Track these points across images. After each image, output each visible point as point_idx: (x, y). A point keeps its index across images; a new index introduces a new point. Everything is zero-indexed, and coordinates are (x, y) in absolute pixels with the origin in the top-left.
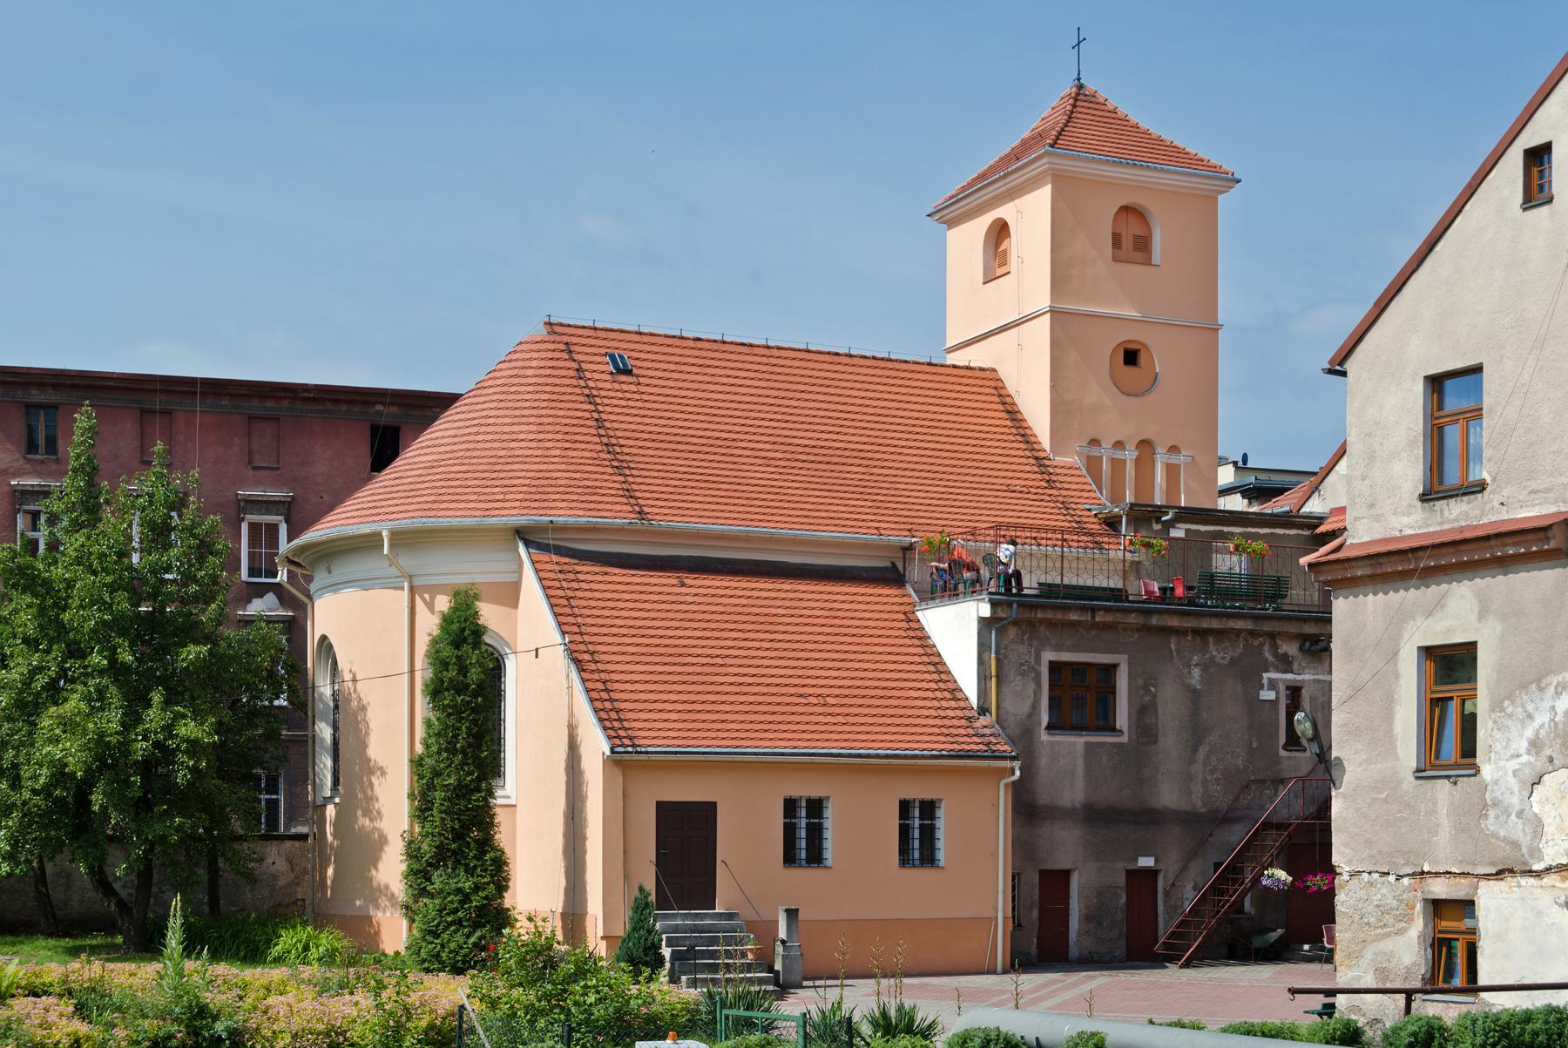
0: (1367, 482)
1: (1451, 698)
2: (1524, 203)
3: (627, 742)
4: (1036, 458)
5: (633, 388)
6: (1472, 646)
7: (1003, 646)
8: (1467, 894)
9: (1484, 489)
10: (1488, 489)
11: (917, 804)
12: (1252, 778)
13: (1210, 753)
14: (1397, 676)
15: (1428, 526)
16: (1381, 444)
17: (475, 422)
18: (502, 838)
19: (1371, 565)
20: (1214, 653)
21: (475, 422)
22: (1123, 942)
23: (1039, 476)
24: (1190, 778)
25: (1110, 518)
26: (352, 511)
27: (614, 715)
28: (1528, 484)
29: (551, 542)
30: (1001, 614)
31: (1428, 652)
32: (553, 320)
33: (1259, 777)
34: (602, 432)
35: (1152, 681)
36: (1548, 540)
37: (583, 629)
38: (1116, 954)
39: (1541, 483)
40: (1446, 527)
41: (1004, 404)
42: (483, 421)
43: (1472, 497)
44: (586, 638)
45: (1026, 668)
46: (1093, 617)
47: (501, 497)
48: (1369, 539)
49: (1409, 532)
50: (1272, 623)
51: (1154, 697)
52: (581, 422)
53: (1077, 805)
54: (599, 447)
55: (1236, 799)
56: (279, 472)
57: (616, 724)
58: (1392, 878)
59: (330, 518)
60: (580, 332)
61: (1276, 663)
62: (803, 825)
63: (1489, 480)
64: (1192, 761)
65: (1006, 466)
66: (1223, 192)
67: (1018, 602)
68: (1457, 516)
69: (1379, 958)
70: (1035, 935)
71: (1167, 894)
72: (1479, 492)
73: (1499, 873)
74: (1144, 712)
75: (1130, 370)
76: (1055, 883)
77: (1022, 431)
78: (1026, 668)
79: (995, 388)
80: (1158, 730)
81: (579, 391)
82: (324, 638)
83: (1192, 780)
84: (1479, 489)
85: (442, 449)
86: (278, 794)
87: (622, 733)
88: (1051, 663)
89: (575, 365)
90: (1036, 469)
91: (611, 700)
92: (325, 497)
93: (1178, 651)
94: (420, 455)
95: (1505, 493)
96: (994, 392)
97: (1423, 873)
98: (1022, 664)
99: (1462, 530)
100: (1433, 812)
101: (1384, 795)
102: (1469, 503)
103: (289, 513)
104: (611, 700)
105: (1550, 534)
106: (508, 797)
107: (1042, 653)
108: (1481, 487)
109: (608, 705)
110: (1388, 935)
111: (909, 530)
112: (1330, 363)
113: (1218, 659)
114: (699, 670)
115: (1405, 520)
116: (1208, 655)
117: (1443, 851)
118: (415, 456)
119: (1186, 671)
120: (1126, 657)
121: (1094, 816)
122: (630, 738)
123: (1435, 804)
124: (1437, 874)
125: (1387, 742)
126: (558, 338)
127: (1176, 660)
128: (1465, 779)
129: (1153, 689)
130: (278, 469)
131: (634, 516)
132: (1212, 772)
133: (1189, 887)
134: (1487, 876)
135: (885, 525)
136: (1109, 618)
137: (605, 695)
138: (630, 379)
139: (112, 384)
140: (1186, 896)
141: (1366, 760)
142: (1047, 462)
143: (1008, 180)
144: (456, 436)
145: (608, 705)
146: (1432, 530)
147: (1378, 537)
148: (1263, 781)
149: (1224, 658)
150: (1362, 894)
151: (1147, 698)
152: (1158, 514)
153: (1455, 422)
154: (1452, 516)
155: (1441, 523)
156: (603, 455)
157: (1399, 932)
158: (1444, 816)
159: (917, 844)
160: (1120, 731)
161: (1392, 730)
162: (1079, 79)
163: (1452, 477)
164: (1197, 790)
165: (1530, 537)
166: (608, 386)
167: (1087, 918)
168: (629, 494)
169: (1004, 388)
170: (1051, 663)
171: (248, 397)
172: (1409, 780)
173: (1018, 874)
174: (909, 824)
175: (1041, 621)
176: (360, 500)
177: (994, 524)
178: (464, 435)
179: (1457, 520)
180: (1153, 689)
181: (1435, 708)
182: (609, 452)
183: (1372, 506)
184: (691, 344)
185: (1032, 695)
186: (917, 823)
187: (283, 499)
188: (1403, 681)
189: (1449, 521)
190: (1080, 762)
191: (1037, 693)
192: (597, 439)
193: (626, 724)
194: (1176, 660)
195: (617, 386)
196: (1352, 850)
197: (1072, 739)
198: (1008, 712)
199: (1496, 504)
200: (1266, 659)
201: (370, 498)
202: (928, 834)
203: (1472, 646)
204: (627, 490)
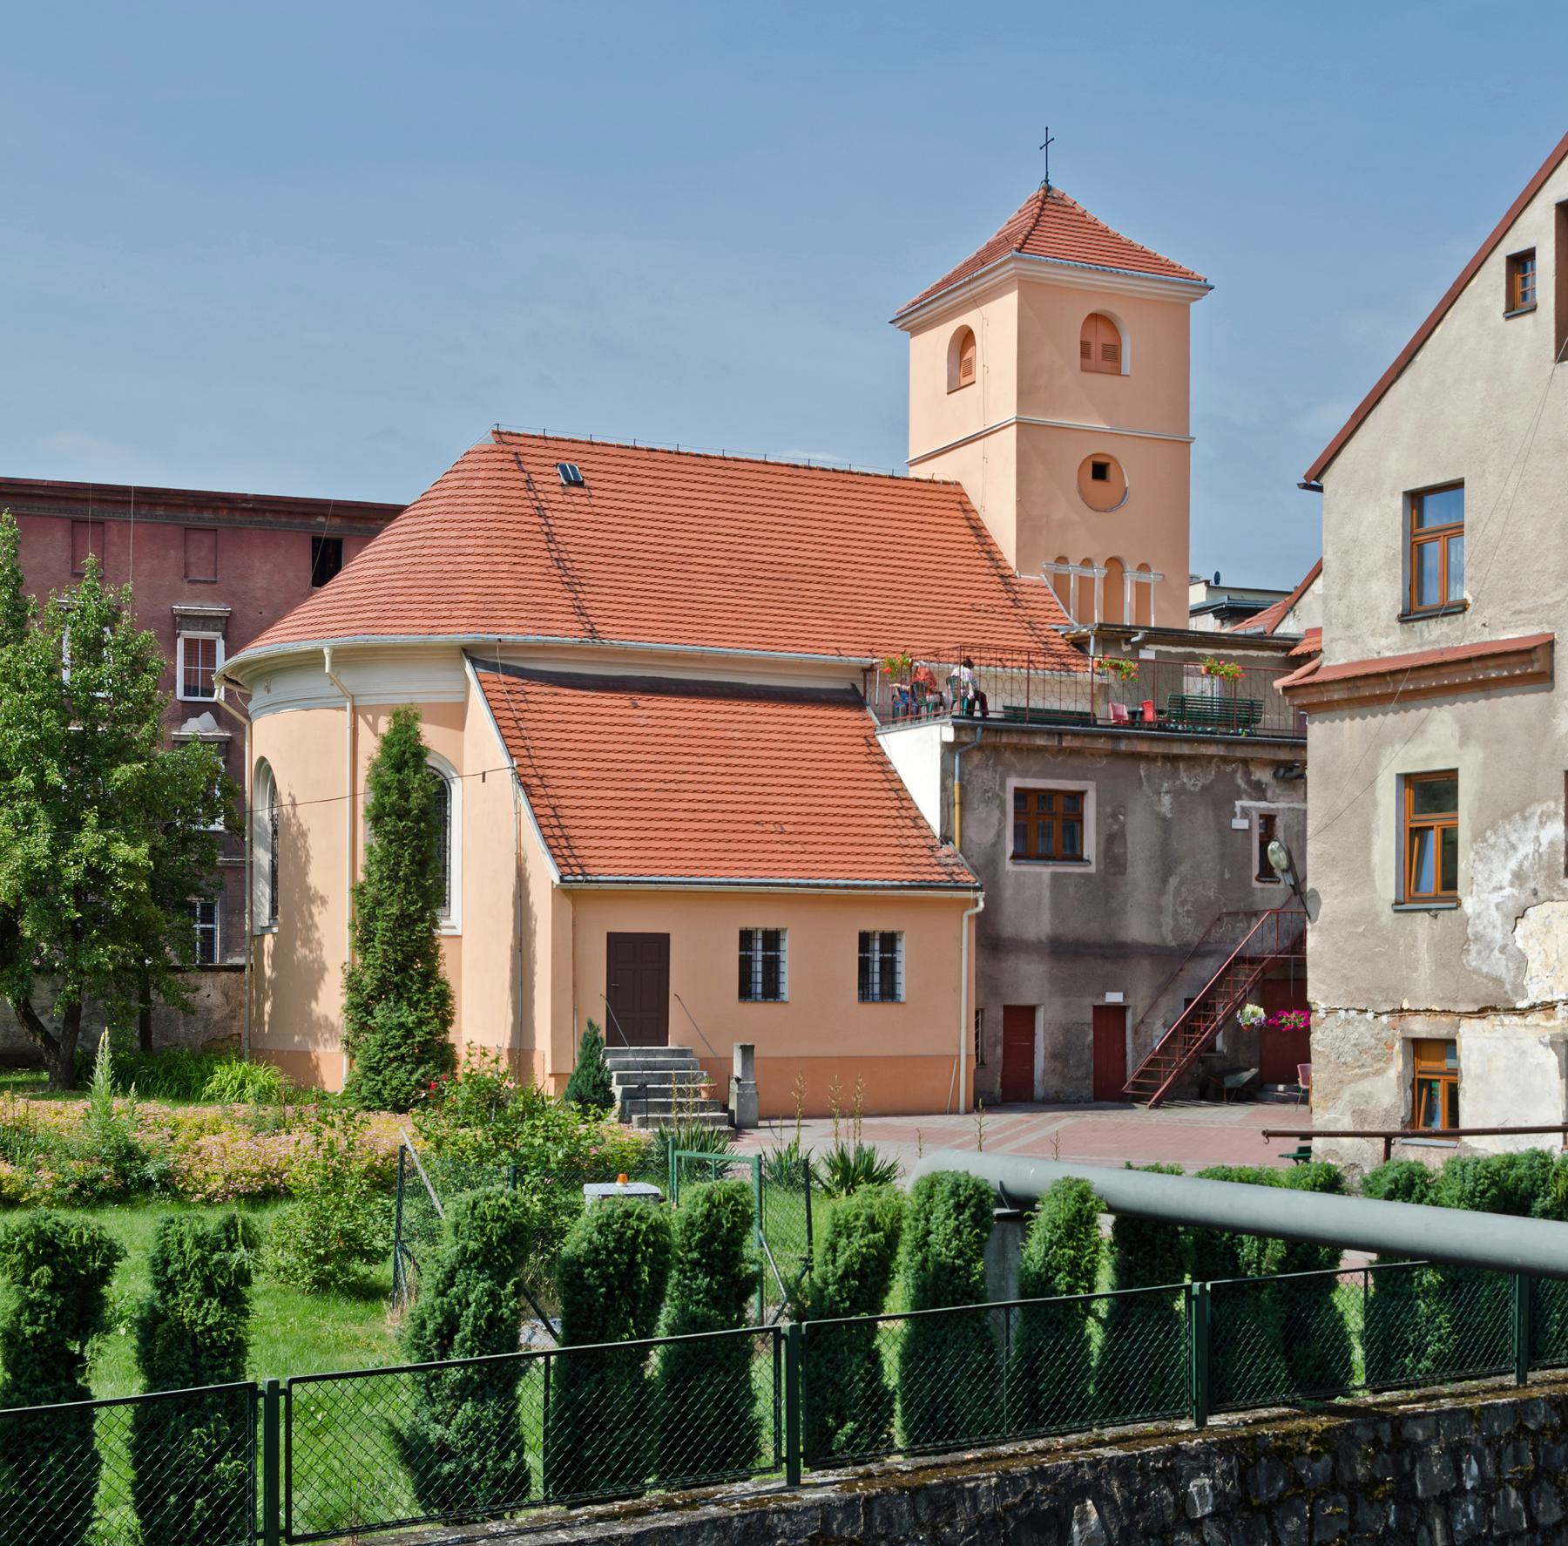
0: (1344, 602)
4: (1002, 576)
6: (1453, 773)
9: (1465, 609)
10: (1470, 610)
13: (1181, 884)
14: (1375, 804)
15: (1407, 648)
16: (1359, 562)
17: (421, 535)
21: (421, 535)
22: (1090, 1082)
23: (1005, 595)
24: (1159, 909)
27: (563, 842)
30: (965, 739)
32: (503, 429)
34: (552, 546)
36: (1532, 662)
37: (532, 752)
41: (968, 519)
42: (429, 534)
43: (1453, 617)
44: (535, 761)
46: (1060, 742)
49: (1387, 654)
51: (1123, 825)
52: (531, 536)
53: (1043, 938)
54: (549, 562)
55: (1208, 933)
56: (215, 586)
58: (1370, 1016)
66: (1195, 300)
67: (982, 726)
68: (1437, 638)
69: (1357, 1100)
71: (1136, 1032)
72: (1460, 612)
74: (1113, 841)
76: (1020, 1019)
79: (960, 503)
82: (262, 760)
87: (572, 861)
88: (1016, 789)
90: (1002, 587)
91: (560, 826)
94: (363, 569)
95: (1487, 613)
96: (959, 507)
97: (1402, 1010)
98: (986, 791)
99: (1442, 652)
105: (1534, 656)
106: (454, 927)
108: (1463, 607)
110: (1366, 1075)
112: (1305, 477)
113: (1189, 787)
115: (1384, 642)
116: (1178, 783)
119: (1155, 798)
120: (1093, 784)
121: (1062, 949)
122: (581, 867)
123: (1415, 938)
124: (1417, 1012)
125: (1362, 873)
126: (507, 448)
128: (1446, 912)
129: (1121, 817)
130: (215, 582)
133: (1159, 1024)
136: (1076, 743)
137: (554, 822)
145: (557, 832)
146: (1411, 651)
148: (1236, 914)
149: (1194, 785)
150: (1339, 1032)
151: (1115, 827)
152: (1127, 635)
155: (1420, 645)
156: (553, 571)
157: (1378, 1072)
158: (1424, 951)
159: (877, 978)
160: (1088, 861)
162: (1047, 181)
163: (1432, 597)
164: (1168, 923)
165: (1513, 659)
166: (559, 498)
167: (1053, 1056)
168: (580, 611)
169: (968, 502)
172: (1387, 913)
173: (982, 1010)
175: (1006, 746)
179: (1437, 641)
180: (1121, 817)
181: (1415, 836)
183: (1349, 627)
184: (645, 455)
188: (1381, 811)
190: (1046, 894)
191: (1002, 821)
192: (547, 554)
193: (576, 852)
195: (567, 498)
199: (1478, 625)
201: (311, 614)
203: (1453, 773)
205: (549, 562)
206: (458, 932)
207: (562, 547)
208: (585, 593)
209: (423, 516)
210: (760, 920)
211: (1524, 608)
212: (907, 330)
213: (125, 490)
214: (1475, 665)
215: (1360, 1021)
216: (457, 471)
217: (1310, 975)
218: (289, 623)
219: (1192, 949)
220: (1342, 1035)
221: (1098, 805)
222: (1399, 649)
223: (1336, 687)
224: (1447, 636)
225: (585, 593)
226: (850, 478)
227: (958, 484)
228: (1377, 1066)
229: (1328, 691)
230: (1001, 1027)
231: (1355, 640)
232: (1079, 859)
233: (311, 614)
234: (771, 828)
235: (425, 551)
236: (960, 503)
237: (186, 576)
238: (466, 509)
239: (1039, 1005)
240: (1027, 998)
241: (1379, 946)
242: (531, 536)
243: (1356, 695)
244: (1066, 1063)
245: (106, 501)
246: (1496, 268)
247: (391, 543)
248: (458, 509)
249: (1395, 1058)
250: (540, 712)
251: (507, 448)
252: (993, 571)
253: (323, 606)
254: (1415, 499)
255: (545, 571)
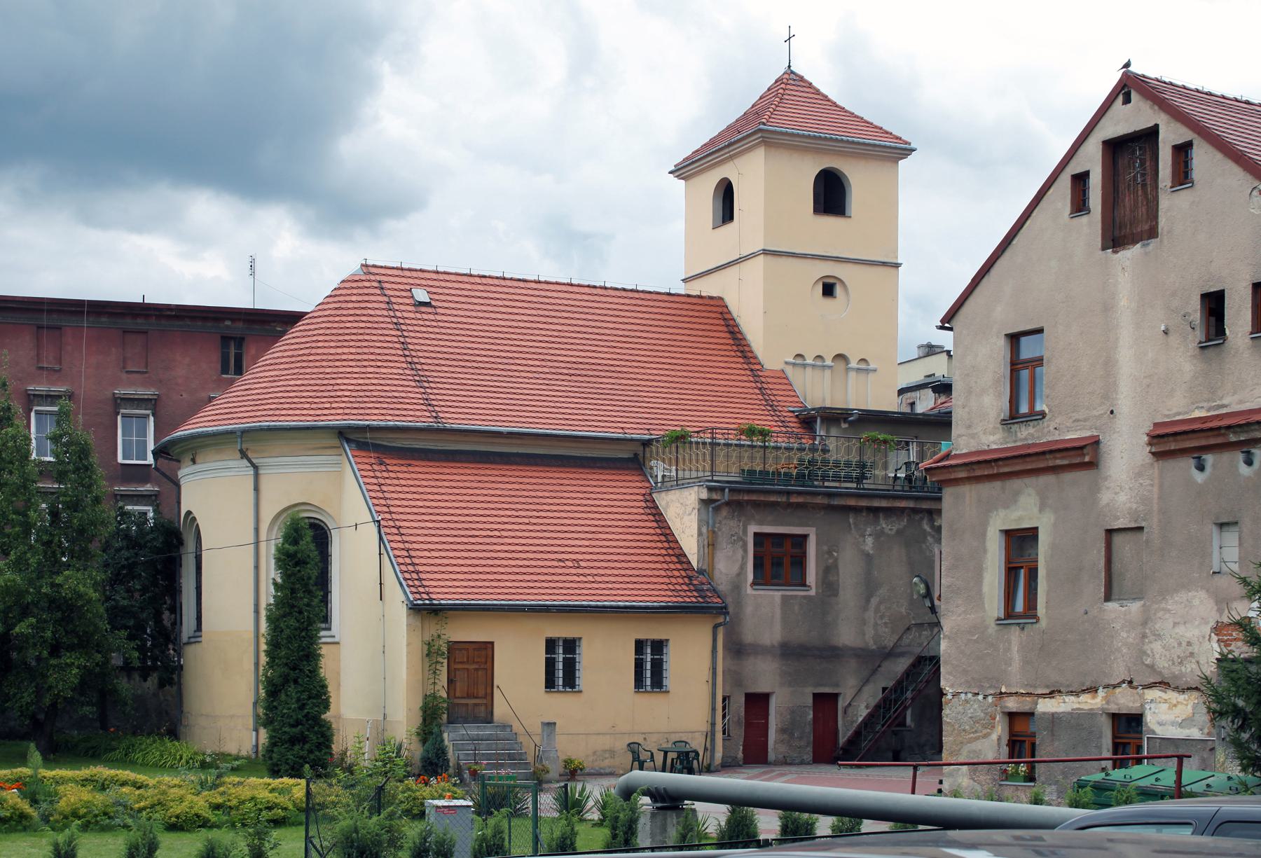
0: (967, 409)
1: (1022, 567)
2: (1071, 214)
3: (425, 596)
4: (752, 370)
5: (432, 317)
6: (1036, 529)
7: (718, 521)
8: (1030, 708)
9: (1044, 417)
10: (1047, 418)
11: (649, 643)
12: (913, 622)
13: (880, 603)
14: (985, 551)
15: (1007, 443)
16: (976, 382)
17: (308, 345)
18: (326, 668)
19: (968, 471)
20: (884, 526)
21: (308, 345)
22: (810, 749)
23: (754, 385)
24: (864, 622)
25: (807, 418)
26: (213, 415)
27: (415, 576)
28: (1074, 414)
29: (370, 441)
30: (715, 496)
31: (1008, 533)
32: (370, 262)
33: (918, 622)
34: (407, 353)
35: (835, 548)
36: (1084, 455)
37: (392, 509)
38: (805, 757)
39: (1080, 415)
40: (1019, 444)
41: (727, 326)
42: (314, 345)
43: (1035, 422)
44: (394, 516)
45: (735, 538)
46: (788, 499)
47: (328, 405)
48: (967, 451)
49: (994, 447)
50: (929, 502)
51: (836, 560)
52: (390, 345)
53: (776, 644)
54: (405, 365)
55: (900, 638)
56: (147, 375)
57: (417, 583)
58: (980, 697)
59: (194, 421)
60: (389, 272)
61: (933, 533)
62: (561, 659)
63: (1047, 412)
64: (865, 608)
65: (727, 377)
66: (902, 159)
67: (729, 487)
68: (1026, 435)
69: (971, 755)
70: (741, 743)
71: (845, 712)
72: (1040, 419)
73: (1050, 693)
74: (829, 571)
75: (828, 302)
76: (757, 703)
77: (741, 348)
78: (735, 538)
79: (721, 313)
80: (839, 585)
81: (388, 320)
82: (189, 513)
83: (865, 624)
84: (1041, 417)
85: (282, 367)
86: (564, 686)
87: (421, 590)
88: (756, 534)
89: (386, 299)
90: (751, 379)
91: (413, 564)
92: (185, 395)
93: (855, 523)
94: (265, 371)
95: (1058, 421)
96: (719, 316)
97: (1001, 693)
98: (732, 535)
99: (1029, 446)
100: (1008, 649)
101: (975, 638)
102: (1034, 427)
103: (155, 408)
104: (413, 564)
105: (1085, 451)
106: (334, 637)
107: (749, 527)
108: (1043, 415)
109: (411, 568)
110: (977, 739)
111: (648, 430)
112: (942, 321)
113: (887, 531)
114: (690, 345)
115: (992, 438)
116: (879, 528)
117: (1015, 676)
118: (261, 372)
119: (861, 540)
120: (814, 529)
121: (789, 652)
122: (428, 594)
123: (1010, 643)
124: (1011, 694)
125: (975, 598)
126: (372, 278)
127: (853, 531)
128: (1030, 625)
129: (835, 554)
130: (146, 372)
131: (432, 420)
132: (882, 617)
133: (863, 706)
134: (1043, 696)
135: (628, 426)
136: (800, 500)
137: (408, 561)
138: (430, 310)
139: (14, 306)
140: (859, 713)
141: (964, 612)
142: (760, 374)
143: (731, 148)
144: (293, 356)
145: (411, 568)
146: (1009, 445)
147: (973, 450)
148: (922, 624)
149: (890, 530)
150: (960, 708)
151: (831, 561)
152: (845, 416)
153: (1027, 368)
154: (1023, 437)
155: (1015, 441)
156: (407, 372)
157: (985, 736)
158: (1015, 653)
159: (648, 674)
160: (809, 586)
161: (981, 591)
162: (789, 67)
163: (1024, 409)
164: (870, 632)
165: (1072, 453)
166: (412, 315)
167: (783, 731)
168: (428, 403)
169: (729, 313)
170: (756, 534)
171: (122, 315)
172: (992, 628)
173: (729, 697)
174: (554, 658)
175: (748, 502)
176: (218, 407)
177: (701, 429)
178: (299, 355)
179: (1026, 439)
180: (835, 554)
181: (1011, 572)
182: (413, 369)
183: (969, 427)
184: (478, 280)
185: (740, 559)
186: (649, 658)
187: (150, 397)
188: (989, 555)
189: (1021, 440)
190: (778, 611)
191: (744, 558)
192: (403, 359)
193: (425, 583)
194: (853, 531)
195: (419, 316)
196: (954, 676)
197: (771, 593)
198: (721, 573)
199: (1051, 428)
200: (925, 530)
201: (225, 406)
202: (658, 668)
203: (1036, 529)
204: (427, 399)
205: (405, 365)
206: (336, 640)
207: (414, 353)
208: (432, 388)
209: (310, 330)
210: (562, 630)
211: (1081, 417)
212: (682, 179)
213: (80, 303)
214: (1048, 456)
215: (975, 701)
216: (336, 296)
217: (942, 669)
218: (209, 411)
219: (887, 651)
220: (962, 711)
221: (817, 544)
222: (1001, 444)
223: (959, 469)
224: (1032, 435)
225: (432, 388)
226: (636, 295)
227: (721, 299)
228: (985, 731)
229: (954, 472)
230: (743, 709)
231: (973, 436)
232: (803, 584)
233: (225, 406)
234: (570, 564)
235: (311, 358)
236: (721, 313)
237: (124, 368)
238: (342, 325)
239: (773, 693)
240: (762, 688)
241: (986, 649)
242: (390, 345)
243: (973, 475)
244: (791, 735)
245: (63, 311)
246: (1065, 182)
247: (286, 351)
248: (336, 325)
249: (996, 726)
250: (398, 479)
251: (372, 278)
252: (746, 367)
253: (234, 399)
254: (1014, 339)
255: (401, 372)
